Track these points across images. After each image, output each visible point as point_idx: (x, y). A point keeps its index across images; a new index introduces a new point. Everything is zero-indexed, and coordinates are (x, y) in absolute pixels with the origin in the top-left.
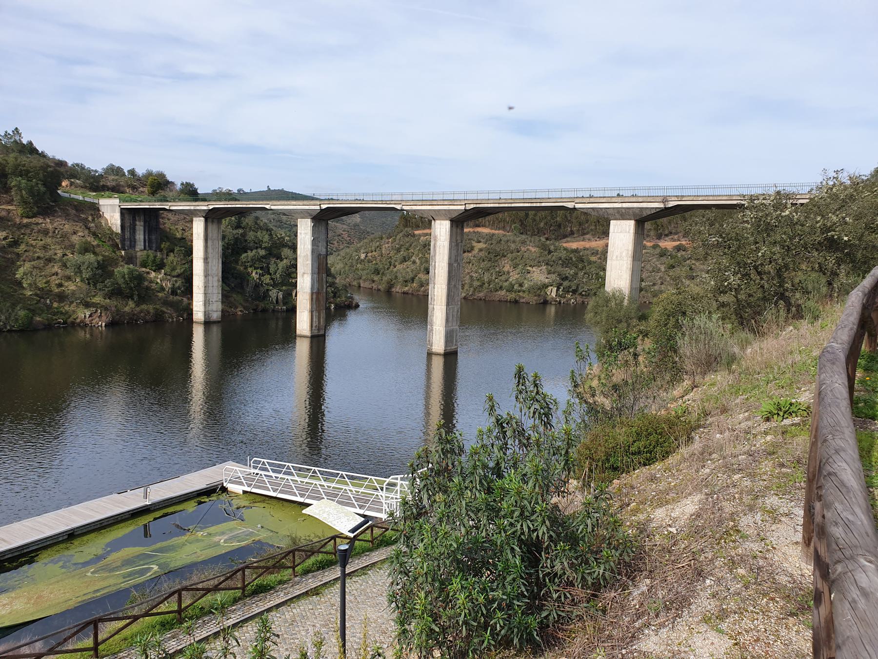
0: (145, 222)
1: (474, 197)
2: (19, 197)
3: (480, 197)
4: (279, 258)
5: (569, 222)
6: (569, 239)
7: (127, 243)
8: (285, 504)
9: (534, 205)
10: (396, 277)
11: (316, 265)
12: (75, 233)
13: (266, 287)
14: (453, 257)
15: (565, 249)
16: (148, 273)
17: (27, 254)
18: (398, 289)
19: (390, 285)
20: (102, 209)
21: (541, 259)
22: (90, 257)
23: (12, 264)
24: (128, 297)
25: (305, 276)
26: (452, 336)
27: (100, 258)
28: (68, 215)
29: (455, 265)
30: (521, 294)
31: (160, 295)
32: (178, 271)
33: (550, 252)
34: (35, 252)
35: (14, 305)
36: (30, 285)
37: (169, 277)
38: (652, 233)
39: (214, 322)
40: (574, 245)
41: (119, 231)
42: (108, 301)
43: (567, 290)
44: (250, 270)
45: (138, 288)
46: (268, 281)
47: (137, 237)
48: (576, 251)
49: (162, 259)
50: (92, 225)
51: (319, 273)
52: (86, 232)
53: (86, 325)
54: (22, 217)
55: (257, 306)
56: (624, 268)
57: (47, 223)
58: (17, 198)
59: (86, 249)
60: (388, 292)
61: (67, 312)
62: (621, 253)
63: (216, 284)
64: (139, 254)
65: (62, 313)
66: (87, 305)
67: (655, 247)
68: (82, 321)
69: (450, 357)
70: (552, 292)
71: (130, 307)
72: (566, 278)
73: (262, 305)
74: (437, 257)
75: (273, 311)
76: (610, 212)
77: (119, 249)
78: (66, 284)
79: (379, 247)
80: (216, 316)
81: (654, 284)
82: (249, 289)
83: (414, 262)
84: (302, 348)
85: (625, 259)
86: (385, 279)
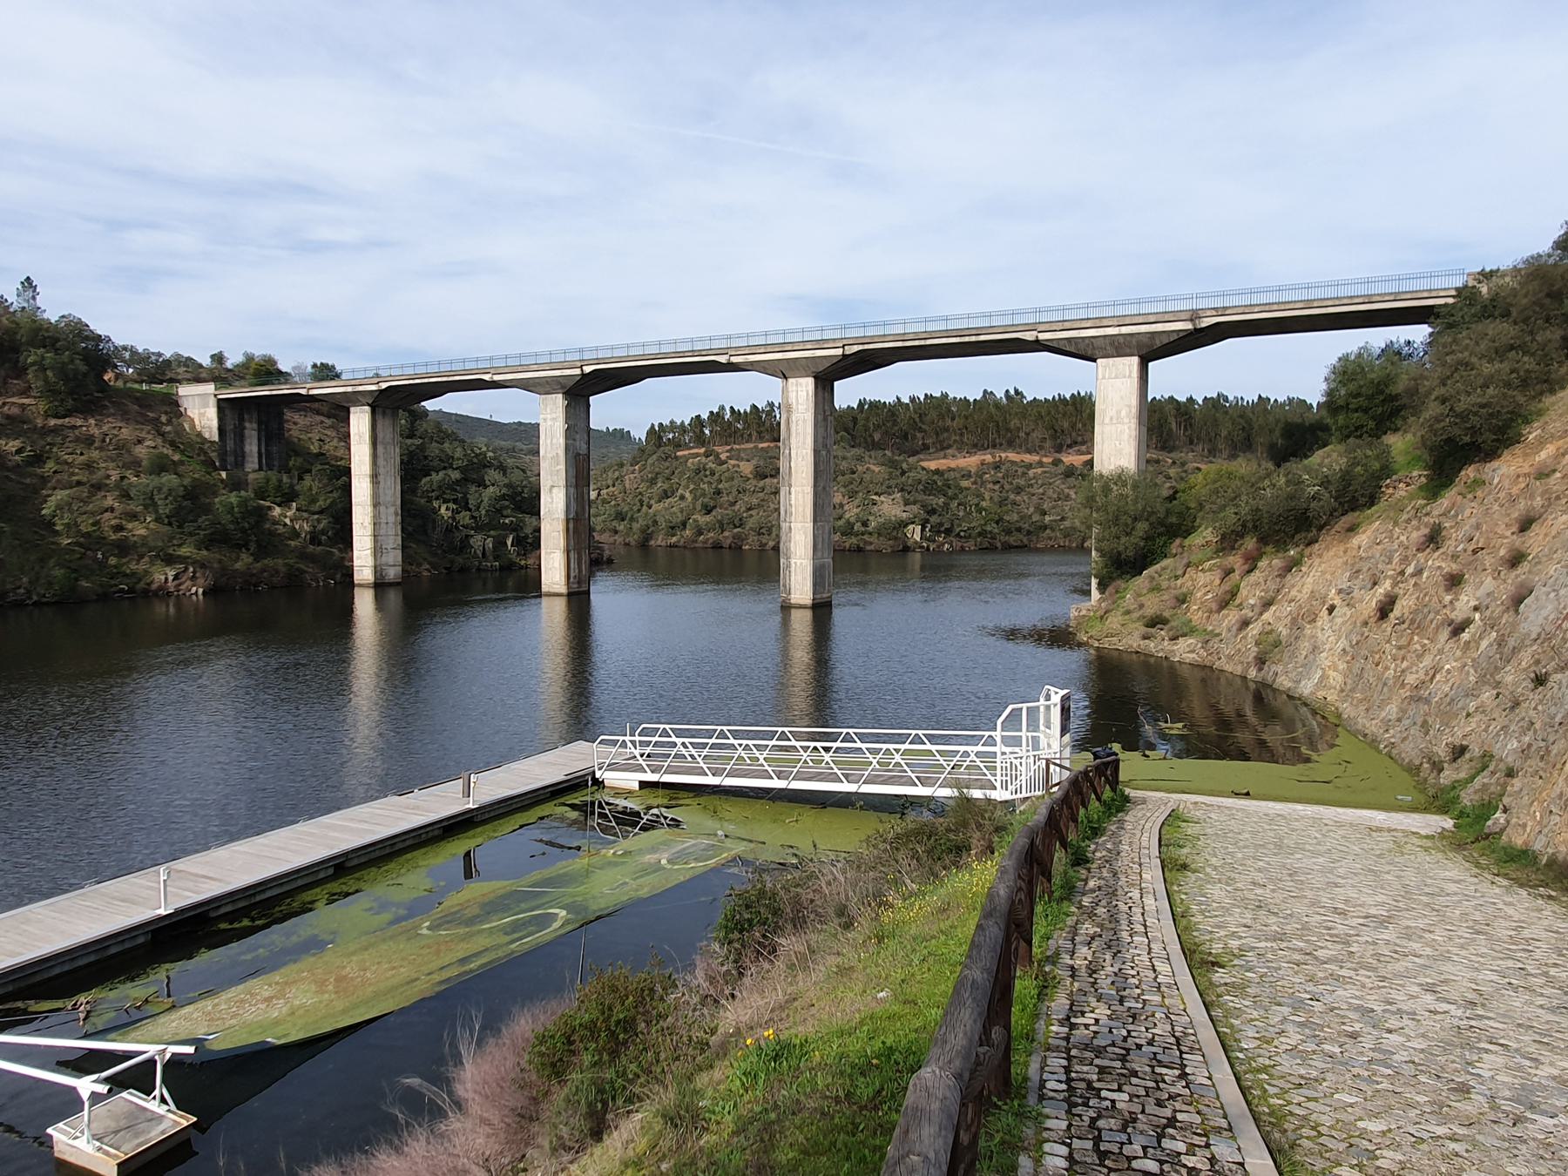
0: (259, 423)
2: (40, 383)
3: (870, 332)
4: (482, 484)
5: (921, 430)
7: (231, 459)
8: (715, 801)
9: (967, 339)
10: (655, 522)
11: (573, 472)
12: (140, 442)
16: (270, 508)
17: (58, 476)
18: (659, 540)
19: (646, 537)
22: (169, 479)
23: (35, 493)
24: (239, 547)
27: (187, 481)
28: (126, 413)
31: (293, 543)
32: (321, 504)
33: (903, 473)
34: (73, 474)
35: (43, 561)
36: (68, 526)
37: (305, 515)
38: (1048, 444)
39: (391, 585)
41: (216, 438)
42: (205, 553)
43: (937, 530)
44: (436, 504)
45: (252, 531)
46: (467, 521)
47: (247, 448)
48: (937, 472)
49: (292, 486)
50: (169, 428)
51: (577, 486)
52: (159, 441)
53: (169, 594)
54: (47, 415)
55: (452, 562)
56: (1126, 437)
57: (91, 426)
60: (644, 545)
61: (133, 574)
62: (1118, 412)
63: (392, 519)
64: (251, 477)
65: (126, 575)
66: (170, 560)
67: (1056, 462)
68: (161, 588)
69: (821, 610)
70: (915, 533)
71: (244, 561)
72: (932, 512)
74: (793, 440)
75: (479, 570)
76: (1097, 343)
77: (216, 469)
78: (130, 526)
79: (620, 478)
80: (393, 573)
81: (1063, 519)
83: (682, 498)
84: (552, 615)
86: (636, 526)
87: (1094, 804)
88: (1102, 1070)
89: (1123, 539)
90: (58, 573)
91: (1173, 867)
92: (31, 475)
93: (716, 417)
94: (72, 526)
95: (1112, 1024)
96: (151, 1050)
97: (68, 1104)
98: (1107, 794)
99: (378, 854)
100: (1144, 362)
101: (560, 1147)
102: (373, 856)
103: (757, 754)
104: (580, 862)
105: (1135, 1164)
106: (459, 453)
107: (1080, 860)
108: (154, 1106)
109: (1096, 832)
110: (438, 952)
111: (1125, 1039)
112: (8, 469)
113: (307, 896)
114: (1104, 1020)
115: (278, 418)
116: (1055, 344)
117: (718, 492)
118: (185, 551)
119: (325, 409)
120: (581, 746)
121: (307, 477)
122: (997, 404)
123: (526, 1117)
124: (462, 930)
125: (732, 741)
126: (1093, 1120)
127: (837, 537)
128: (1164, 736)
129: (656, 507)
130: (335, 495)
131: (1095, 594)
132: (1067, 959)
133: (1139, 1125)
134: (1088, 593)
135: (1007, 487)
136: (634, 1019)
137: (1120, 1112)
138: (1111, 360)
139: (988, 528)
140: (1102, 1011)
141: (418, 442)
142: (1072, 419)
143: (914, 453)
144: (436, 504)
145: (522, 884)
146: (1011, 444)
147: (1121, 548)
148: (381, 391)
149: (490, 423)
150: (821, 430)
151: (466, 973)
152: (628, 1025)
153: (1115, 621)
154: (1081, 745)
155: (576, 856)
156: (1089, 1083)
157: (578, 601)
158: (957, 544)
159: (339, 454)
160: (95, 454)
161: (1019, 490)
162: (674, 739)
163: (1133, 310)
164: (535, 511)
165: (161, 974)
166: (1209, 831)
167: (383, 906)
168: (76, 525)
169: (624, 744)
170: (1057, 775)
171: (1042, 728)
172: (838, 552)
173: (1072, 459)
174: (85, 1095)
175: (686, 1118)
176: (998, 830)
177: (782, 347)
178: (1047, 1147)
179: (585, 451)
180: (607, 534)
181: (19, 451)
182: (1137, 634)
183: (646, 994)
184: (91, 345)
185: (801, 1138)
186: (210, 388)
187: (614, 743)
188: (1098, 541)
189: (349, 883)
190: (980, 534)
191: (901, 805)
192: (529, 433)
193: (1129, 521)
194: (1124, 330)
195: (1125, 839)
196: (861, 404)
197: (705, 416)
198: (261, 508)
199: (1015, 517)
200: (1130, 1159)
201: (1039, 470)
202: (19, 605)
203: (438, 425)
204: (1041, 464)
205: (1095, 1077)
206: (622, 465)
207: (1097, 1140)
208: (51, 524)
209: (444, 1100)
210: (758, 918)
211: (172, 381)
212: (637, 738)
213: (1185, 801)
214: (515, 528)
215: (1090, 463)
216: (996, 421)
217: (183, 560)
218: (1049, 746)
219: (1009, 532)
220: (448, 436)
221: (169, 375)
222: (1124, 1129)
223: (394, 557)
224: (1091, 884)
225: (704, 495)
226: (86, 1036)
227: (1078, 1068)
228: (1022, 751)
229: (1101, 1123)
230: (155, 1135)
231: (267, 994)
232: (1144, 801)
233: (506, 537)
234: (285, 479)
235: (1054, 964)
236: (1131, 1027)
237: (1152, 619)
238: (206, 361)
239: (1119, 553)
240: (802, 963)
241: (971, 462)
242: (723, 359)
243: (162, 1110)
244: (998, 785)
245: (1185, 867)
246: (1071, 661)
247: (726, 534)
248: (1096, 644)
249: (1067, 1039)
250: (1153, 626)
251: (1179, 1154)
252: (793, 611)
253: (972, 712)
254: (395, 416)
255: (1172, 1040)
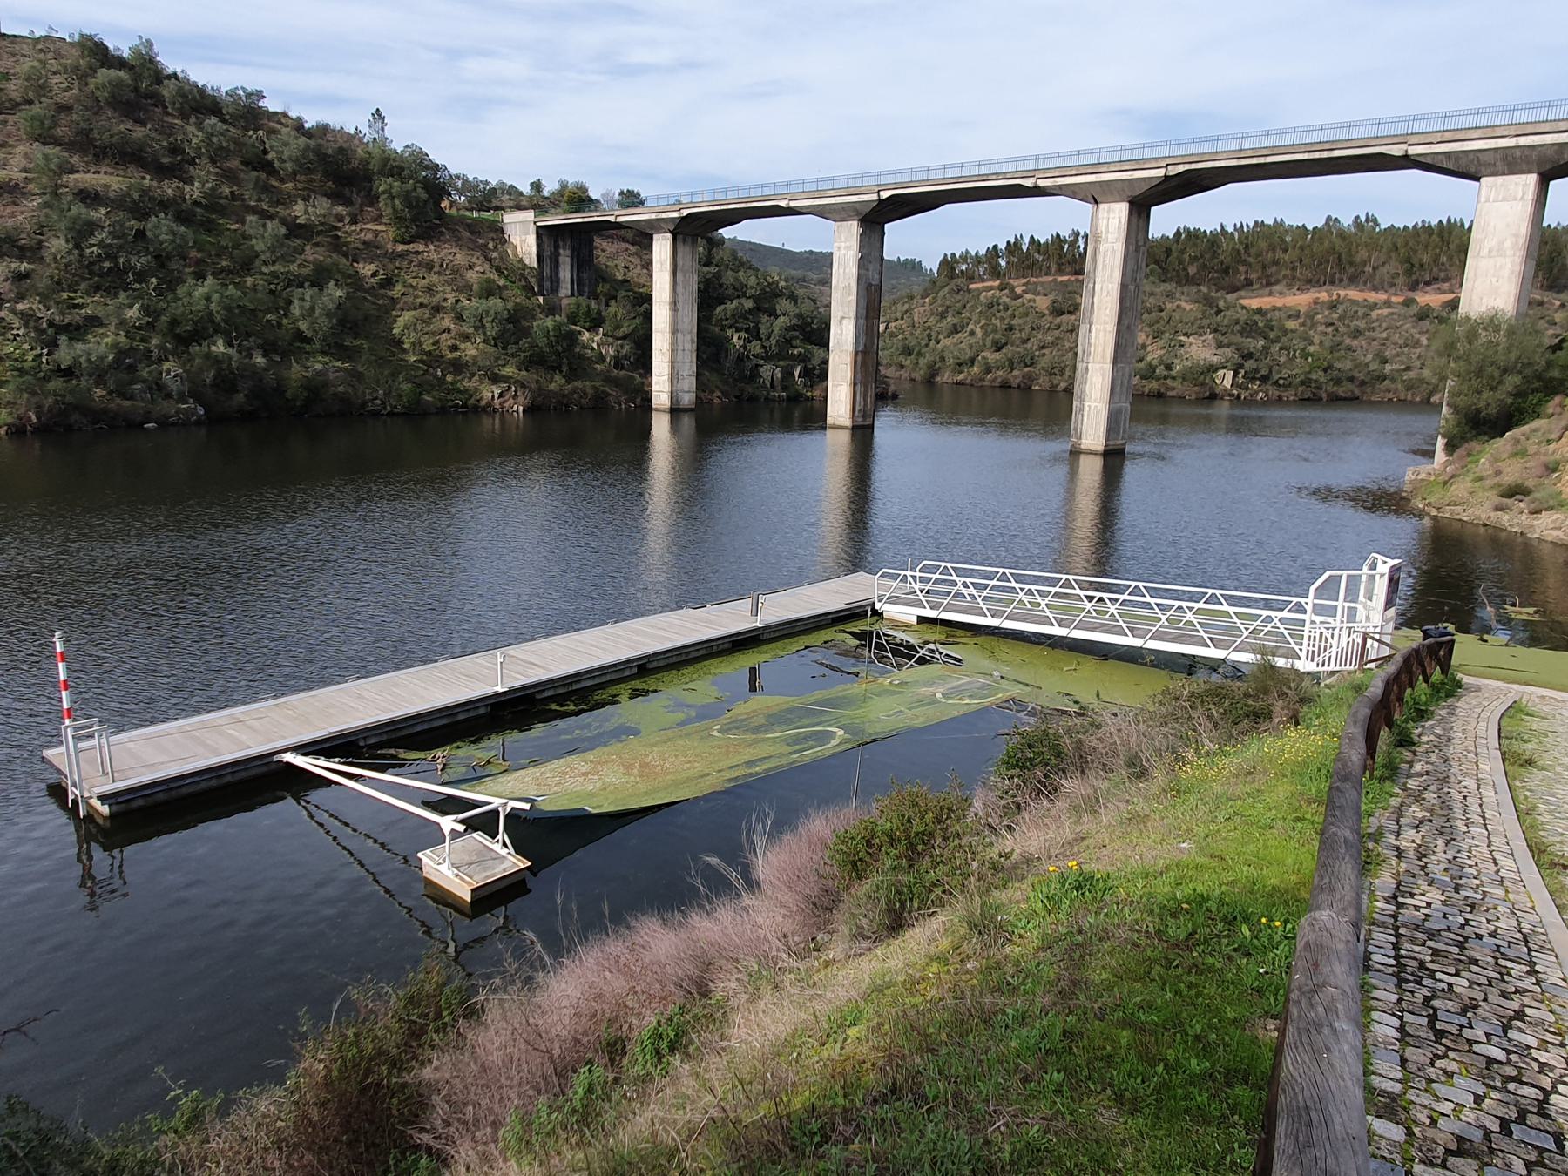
1: (1185, 150)
2: (389, 210)
3: (1199, 149)
5: (1245, 263)
6: (1242, 293)
7: (547, 284)
8: (994, 642)
9: (1317, 155)
10: (942, 358)
11: (863, 303)
12: (471, 267)
13: (755, 361)
14: (1129, 273)
15: (1243, 307)
17: (405, 298)
18: (946, 377)
19: (933, 372)
20: (509, 230)
21: (1205, 322)
22: (495, 303)
24: (554, 369)
25: (845, 322)
26: (1117, 422)
27: (510, 306)
28: (459, 239)
29: (1132, 288)
30: (1168, 381)
32: (625, 329)
33: (1219, 312)
34: (417, 297)
35: (394, 375)
36: (413, 344)
38: (1400, 280)
39: (686, 410)
40: (1254, 303)
43: (1251, 377)
44: (729, 332)
45: (563, 355)
46: (758, 350)
47: (561, 275)
48: (1259, 311)
49: (599, 312)
50: (495, 255)
51: (867, 318)
52: (487, 266)
55: (742, 390)
56: (1506, 272)
57: (430, 252)
58: (387, 211)
59: (489, 291)
60: (930, 381)
62: (1501, 243)
63: (688, 346)
64: (565, 302)
65: (460, 392)
66: (495, 379)
67: (1408, 303)
68: (489, 404)
69: (1113, 458)
70: (1225, 379)
71: (557, 383)
72: (1249, 356)
73: (749, 389)
77: (535, 294)
78: (463, 346)
80: (688, 399)
81: (1408, 369)
82: (728, 364)
83: (972, 333)
84: (836, 444)
85: (1509, 253)
86: (922, 361)
87: (1421, 685)
88: (1436, 953)
89: (1486, 394)
90: (406, 387)
91: (1517, 761)
92: (383, 296)
93: (1014, 247)
94: (417, 344)
95: (1446, 909)
96: (496, 802)
97: (435, 837)
98: (1437, 675)
99: (674, 660)
100: (1545, 179)
101: (859, 935)
102: (671, 661)
103: (1039, 599)
104: (858, 687)
105: (1476, 1048)
106: (752, 281)
107: (1405, 741)
108: (497, 847)
109: (1422, 714)
110: (727, 752)
111: (1462, 927)
112: (366, 291)
113: (613, 690)
114: (1437, 905)
115: (588, 241)
116: (1429, 160)
117: (1010, 329)
118: (509, 371)
119: (630, 235)
120: (861, 577)
121: (613, 303)
122: (1342, 235)
123: (823, 907)
124: (749, 736)
125: (1013, 584)
126: (1427, 1001)
127: (1136, 380)
128: (1506, 621)
129: (944, 342)
130: (637, 321)
131: (1440, 455)
132: (1392, 840)
133: (1479, 1012)
134: (1430, 455)
135: (1342, 329)
136: (931, 834)
137: (1458, 996)
138: (1500, 179)
139: (1314, 377)
140: (1435, 896)
141: (713, 269)
142: (1440, 251)
143: (1235, 289)
144: (729, 332)
145: (803, 702)
146: (1353, 280)
147: (1482, 404)
148: (683, 218)
149: (782, 252)
150: (1131, 263)
151: (751, 775)
152: (926, 837)
153: (1466, 489)
154: (1406, 621)
155: (853, 682)
156: (1422, 965)
157: (862, 433)
158: (1274, 392)
159: (641, 281)
160: (435, 278)
161: (1357, 333)
162: (954, 578)
163: (1540, 115)
164: (824, 344)
165: (495, 741)
166: (1560, 728)
167: (681, 705)
168: (420, 344)
169: (905, 579)
170: (1374, 649)
171: (1361, 598)
172: (1138, 397)
173: (1430, 298)
174: (447, 831)
175: (985, 926)
176: (1302, 701)
177: (1096, 168)
178: (1375, 1015)
179: (877, 282)
180: (893, 369)
181: (374, 275)
182: (1488, 505)
183: (945, 813)
184: (430, 174)
185: (1113, 962)
186: (530, 215)
187: (895, 577)
188: (1453, 394)
189: (650, 683)
190: (1302, 383)
191: (1189, 665)
192: (821, 263)
193: (1497, 374)
194: (1523, 141)
195: (1458, 726)
196: (1178, 233)
197: (1002, 246)
198: (572, 332)
199: (1348, 365)
200: (1471, 1042)
201: (1385, 311)
202: (375, 414)
203: (734, 253)
204: (1388, 304)
205: (1428, 958)
206: (912, 298)
207: (1433, 1018)
208: (400, 343)
209: (736, 877)
210: (1042, 758)
211: (497, 208)
212: (918, 574)
213: (1531, 694)
214: (803, 359)
215: (1454, 305)
216: (1335, 254)
217: (506, 379)
218: (1368, 619)
219: (1338, 382)
220: (743, 264)
221: (495, 203)
222: (1463, 1012)
223: (689, 384)
224: (1418, 767)
225: (995, 331)
226: (443, 784)
227: (1407, 946)
228: (1335, 622)
229: (1436, 1003)
230: (499, 871)
231: (583, 770)
232: (1478, 689)
233: (793, 368)
234: (594, 305)
235: (1376, 841)
236: (1468, 916)
237: (1510, 487)
238: (526, 189)
239: (1478, 411)
240: (1092, 804)
241: (1300, 300)
242: (1029, 183)
243: (504, 852)
244: (1303, 655)
245: (1530, 762)
246: (1404, 531)
247: (1016, 372)
248: (1434, 512)
249: (1395, 917)
250: (1511, 496)
251: (1529, 1047)
252: (1082, 457)
253: (1283, 578)
254: (694, 242)
255: (1519, 936)
